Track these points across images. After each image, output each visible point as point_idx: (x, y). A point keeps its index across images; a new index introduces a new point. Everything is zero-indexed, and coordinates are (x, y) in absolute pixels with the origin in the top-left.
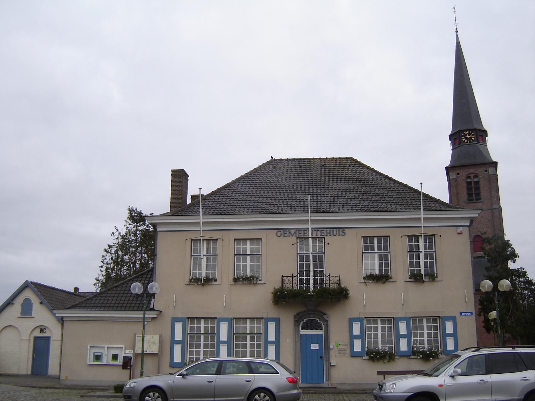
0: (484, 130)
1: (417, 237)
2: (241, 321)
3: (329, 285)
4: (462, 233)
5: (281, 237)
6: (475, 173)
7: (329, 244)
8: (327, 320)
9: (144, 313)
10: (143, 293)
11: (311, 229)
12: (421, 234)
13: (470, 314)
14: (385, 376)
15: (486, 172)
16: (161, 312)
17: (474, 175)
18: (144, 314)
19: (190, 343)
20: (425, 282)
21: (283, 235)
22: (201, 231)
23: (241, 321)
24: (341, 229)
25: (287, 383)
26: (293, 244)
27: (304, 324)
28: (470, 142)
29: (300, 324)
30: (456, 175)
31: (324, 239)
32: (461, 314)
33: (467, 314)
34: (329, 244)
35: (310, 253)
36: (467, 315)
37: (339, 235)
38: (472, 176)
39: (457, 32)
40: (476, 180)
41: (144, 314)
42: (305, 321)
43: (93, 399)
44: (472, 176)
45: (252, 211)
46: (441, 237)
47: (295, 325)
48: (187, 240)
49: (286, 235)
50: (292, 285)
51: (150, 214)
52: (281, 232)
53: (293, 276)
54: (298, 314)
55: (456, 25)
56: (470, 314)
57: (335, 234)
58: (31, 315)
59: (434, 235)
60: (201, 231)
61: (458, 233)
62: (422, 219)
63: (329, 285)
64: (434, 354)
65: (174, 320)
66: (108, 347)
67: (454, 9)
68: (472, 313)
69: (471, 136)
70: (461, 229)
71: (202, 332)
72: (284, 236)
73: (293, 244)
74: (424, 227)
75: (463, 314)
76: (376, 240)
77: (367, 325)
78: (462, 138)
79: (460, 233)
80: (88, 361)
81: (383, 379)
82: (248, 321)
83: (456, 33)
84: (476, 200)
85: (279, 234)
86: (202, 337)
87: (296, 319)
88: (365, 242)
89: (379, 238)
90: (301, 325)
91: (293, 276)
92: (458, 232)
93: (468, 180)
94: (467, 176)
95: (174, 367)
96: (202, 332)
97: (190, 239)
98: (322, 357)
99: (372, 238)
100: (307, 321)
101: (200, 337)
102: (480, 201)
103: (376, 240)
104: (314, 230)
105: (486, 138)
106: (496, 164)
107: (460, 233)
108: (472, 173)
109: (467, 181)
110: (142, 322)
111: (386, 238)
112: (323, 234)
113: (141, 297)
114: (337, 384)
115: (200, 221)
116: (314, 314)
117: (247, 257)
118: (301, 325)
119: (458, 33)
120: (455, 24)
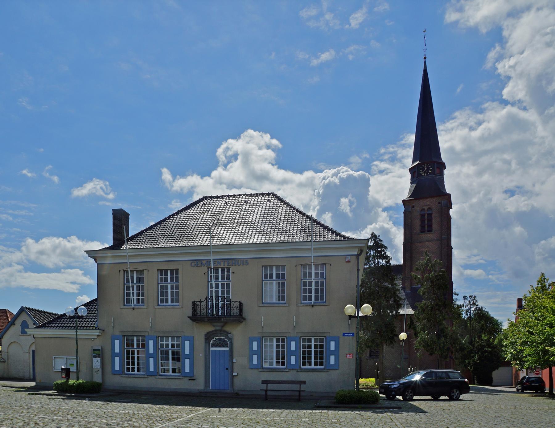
0: (441, 162)
1: (166, 271)
2: (176, 338)
3: (201, 309)
4: (350, 262)
5: (195, 267)
6: (429, 205)
7: (234, 273)
8: (231, 339)
9: (76, 331)
11: (213, 260)
12: (311, 263)
13: (352, 335)
14: (268, 384)
15: (440, 205)
16: (104, 331)
17: (428, 207)
18: (76, 332)
19: (323, 343)
20: (314, 307)
21: (196, 266)
22: (312, 257)
23: (176, 338)
24: (245, 260)
26: (204, 274)
28: (427, 174)
29: (210, 342)
30: (411, 208)
31: (325, 265)
32: (344, 335)
33: (349, 335)
34: (234, 273)
35: (313, 279)
36: (349, 336)
37: (243, 265)
39: (425, 58)
40: (430, 212)
41: (76, 332)
44: (426, 208)
45: (181, 243)
46: (331, 265)
47: (206, 342)
48: (297, 266)
49: (198, 265)
50: (200, 309)
52: (195, 263)
53: (201, 301)
55: (425, 51)
56: (352, 335)
57: (239, 263)
59: (325, 264)
60: (312, 257)
61: (346, 262)
62: (211, 252)
63: (201, 309)
65: (114, 338)
66: (67, 358)
67: (425, 32)
68: (353, 334)
70: (349, 258)
72: (197, 267)
73: (204, 274)
74: (314, 256)
75: (345, 335)
76: (274, 268)
77: (308, 339)
78: (420, 171)
79: (348, 262)
80: (54, 369)
83: (424, 60)
84: (428, 231)
85: (193, 264)
87: (206, 338)
88: (161, 274)
89: (172, 271)
91: (201, 301)
92: (346, 261)
93: (423, 213)
94: (421, 208)
95: (115, 374)
97: (122, 271)
98: (227, 369)
99: (166, 271)
100: (216, 339)
102: (431, 232)
103: (274, 268)
104: (222, 260)
105: (332, 169)
106: (450, 195)
107: (348, 262)
109: (421, 213)
110: (75, 339)
111: (142, 271)
112: (229, 264)
113: (409, 303)
114: (238, 390)
115: (210, 251)
116: (220, 333)
117: (273, 283)
118: (211, 342)
119: (426, 60)
120: (424, 50)
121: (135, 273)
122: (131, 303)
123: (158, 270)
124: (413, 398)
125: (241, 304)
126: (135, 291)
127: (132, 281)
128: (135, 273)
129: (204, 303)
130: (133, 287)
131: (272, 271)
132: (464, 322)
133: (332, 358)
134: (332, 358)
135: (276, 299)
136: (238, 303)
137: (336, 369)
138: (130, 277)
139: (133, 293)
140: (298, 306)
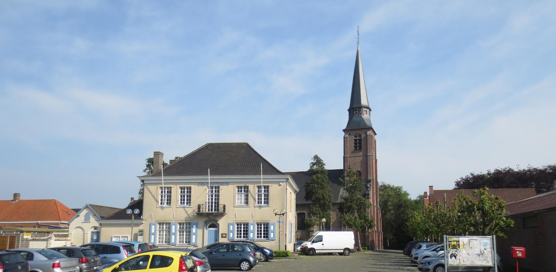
10: (132, 213)
17: (359, 135)
25: (501, 262)
27: (209, 225)
38: (357, 135)
42: (210, 224)
43: (450, 262)
44: (357, 135)
51: (388, 184)
54: (206, 221)
58: (90, 221)
64: (519, 252)
69: (358, 113)
71: (164, 229)
76: (185, 224)
81: (283, 260)
82: (165, 224)
84: (359, 150)
86: (165, 231)
90: (208, 226)
96: (164, 229)
100: (211, 224)
101: (184, 231)
103: (185, 224)
108: (358, 134)
121: (166, 188)
122: (163, 204)
123: (180, 187)
124: (27, 253)
125: (224, 206)
126: (166, 198)
127: (165, 193)
128: (166, 188)
129: (204, 206)
130: (165, 196)
131: (184, 225)
132: (486, 185)
133: (272, 234)
134: (272, 234)
135: (244, 202)
136: (223, 205)
137: (274, 240)
138: (164, 191)
139: (165, 199)
140: (255, 207)
